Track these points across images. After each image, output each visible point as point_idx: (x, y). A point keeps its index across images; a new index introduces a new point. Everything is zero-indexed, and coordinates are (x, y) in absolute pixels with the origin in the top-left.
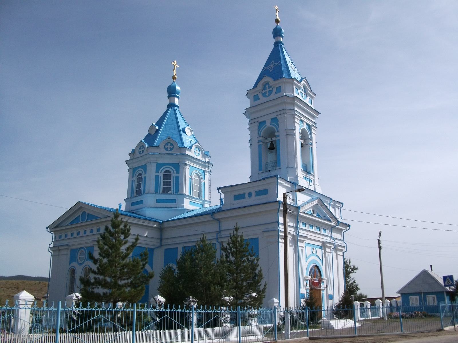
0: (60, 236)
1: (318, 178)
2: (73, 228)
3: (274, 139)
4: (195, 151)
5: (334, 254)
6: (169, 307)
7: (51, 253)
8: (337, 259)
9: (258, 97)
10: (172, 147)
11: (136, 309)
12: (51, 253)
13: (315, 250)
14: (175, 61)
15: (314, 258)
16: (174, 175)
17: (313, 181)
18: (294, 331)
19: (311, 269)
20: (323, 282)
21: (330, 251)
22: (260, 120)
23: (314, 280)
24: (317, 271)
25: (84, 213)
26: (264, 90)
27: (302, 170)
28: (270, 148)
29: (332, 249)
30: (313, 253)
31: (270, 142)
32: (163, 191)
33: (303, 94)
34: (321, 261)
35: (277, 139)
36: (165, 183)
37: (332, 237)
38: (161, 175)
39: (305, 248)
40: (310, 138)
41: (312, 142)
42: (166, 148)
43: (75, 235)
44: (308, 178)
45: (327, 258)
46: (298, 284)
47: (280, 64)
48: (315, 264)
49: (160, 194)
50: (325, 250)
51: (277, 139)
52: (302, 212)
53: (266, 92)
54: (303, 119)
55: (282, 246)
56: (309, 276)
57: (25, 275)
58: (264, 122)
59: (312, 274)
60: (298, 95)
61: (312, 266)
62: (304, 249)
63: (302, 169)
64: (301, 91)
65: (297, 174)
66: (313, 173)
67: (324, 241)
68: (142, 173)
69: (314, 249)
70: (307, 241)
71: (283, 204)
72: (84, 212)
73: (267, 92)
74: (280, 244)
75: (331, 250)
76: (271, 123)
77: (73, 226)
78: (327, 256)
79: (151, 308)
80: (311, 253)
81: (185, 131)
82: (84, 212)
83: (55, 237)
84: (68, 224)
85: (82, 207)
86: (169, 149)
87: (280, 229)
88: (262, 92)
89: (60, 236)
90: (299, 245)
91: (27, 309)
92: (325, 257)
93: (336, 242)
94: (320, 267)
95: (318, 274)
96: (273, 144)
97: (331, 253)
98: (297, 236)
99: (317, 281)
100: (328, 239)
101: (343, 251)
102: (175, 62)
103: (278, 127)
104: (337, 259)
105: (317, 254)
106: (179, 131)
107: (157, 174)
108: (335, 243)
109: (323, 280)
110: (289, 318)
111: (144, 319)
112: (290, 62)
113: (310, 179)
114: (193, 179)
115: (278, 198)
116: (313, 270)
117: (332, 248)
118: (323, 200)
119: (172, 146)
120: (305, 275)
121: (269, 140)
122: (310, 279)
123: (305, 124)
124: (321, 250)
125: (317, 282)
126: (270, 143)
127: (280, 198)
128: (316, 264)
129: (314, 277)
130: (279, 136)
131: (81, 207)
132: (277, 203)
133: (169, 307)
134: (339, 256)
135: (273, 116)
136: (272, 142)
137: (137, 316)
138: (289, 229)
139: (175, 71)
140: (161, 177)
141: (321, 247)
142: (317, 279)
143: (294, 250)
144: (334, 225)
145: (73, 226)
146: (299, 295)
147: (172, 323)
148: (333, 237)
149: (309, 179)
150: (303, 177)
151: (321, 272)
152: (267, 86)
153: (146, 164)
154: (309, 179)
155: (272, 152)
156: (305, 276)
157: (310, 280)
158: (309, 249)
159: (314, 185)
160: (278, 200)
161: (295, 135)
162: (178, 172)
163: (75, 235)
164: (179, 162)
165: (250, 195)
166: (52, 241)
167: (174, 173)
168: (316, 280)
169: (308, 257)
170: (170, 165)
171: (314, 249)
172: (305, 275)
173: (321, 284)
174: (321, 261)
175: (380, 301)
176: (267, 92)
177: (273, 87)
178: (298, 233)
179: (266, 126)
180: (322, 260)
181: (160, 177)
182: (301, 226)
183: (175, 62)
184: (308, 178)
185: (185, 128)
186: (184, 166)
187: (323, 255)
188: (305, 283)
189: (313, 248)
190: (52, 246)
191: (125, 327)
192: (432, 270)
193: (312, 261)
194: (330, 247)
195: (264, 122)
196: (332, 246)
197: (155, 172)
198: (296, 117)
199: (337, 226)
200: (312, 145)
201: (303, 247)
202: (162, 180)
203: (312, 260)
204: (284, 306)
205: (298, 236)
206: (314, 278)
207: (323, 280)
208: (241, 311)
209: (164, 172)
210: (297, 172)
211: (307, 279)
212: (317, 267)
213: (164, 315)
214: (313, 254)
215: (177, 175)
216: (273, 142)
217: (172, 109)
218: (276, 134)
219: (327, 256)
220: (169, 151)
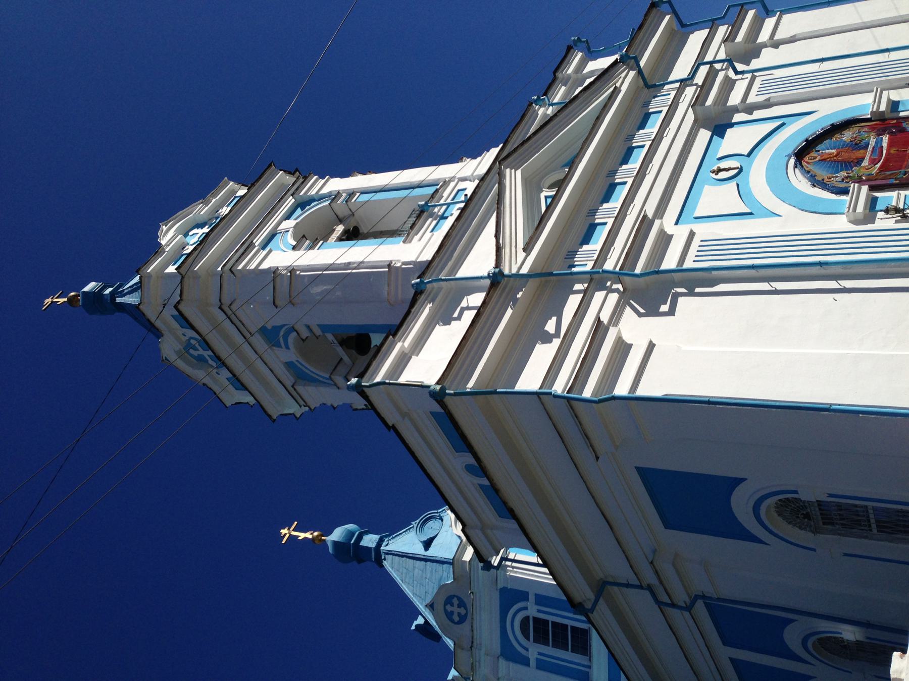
5: (768, 57)
8: (792, 40)
10: (455, 601)
13: (724, 164)
19: (816, 182)
20: (894, 105)
22: (289, 380)
23: (873, 162)
24: (827, 149)
26: (208, 361)
30: (735, 171)
34: (783, 124)
36: (560, 643)
38: (534, 651)
40: (327, 203)
41: (344, 191)
42: (462, 608)
48: (792, 161)
49: (589, 667)
52: (524, 254)
56: (845, 192)
58: (289, 365)
59: (843, 174)
61: (799, 182)
62: (704, 231)
69: (720, 170)
75: (740, 76)
78: (761, 98)
80: (732, 185)
92: (767, 105)
94: (809, 134)
95: (847, 136)
97: (756, 74)
98: (627, 279)
99: (885, 139)
104: (792, 40)
105: (746, 154)
107: (533, 663)
109: (883, 108)
113: (449, 201)
116: (822, 173)
118: (511, 148)
120: (841, 223)
122: (865, 188)
125: (890, 145)
128: (790, 157)
129: (859, 161)
135: (258, 341)
140: (540, 654)
141: (720, 130)
142: (872, 142)
143: (697, 290)
144: (632, 74)
146: (421, 613)
149: (448, 205)
151: (837, 120)
157: (872, 188)
162: (524, 596)
167: (526, 608)
168: (878, 148)
170: (505, 622)
171: (720, 170)
172: (841, 223)
173: (902, 114)
174: (783, 124)
180: (778, 123)
182: (585, 260)
184: (444, 207)
186: (506, 571)
187: (757, 114)
188: (884, 222)
194: (729, 85)
195: (289, 365)
200: (351, 194)
201: (692, 235)
205: (624, 273)
206: (866, 163)
207: (883, 108)
210: (404, 263)
212: (800, 155)
214: (741, 170)
215: (532, 598)
217: (385, 559)
219: (767, 96)
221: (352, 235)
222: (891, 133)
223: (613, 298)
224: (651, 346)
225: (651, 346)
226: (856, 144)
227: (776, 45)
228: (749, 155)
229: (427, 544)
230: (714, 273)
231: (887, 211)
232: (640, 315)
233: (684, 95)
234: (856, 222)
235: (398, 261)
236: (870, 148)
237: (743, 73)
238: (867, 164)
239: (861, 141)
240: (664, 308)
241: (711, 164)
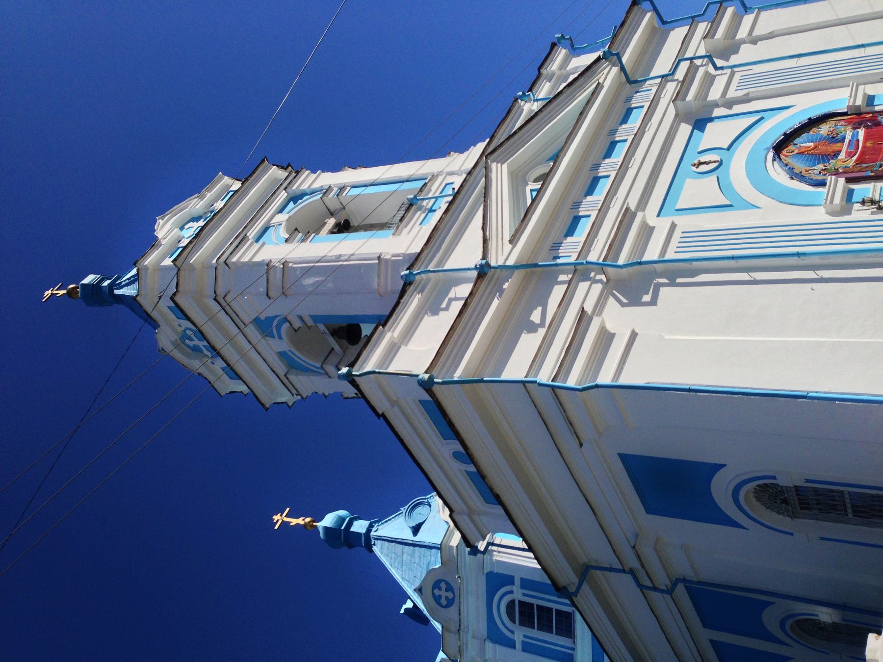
1: (296, 229)
5: (746, 53)
13: (704, 158)
16: (518, 594)
21: (725, 78)
22: (281, 369)
23: (850, 155)
24: (804, 142)
27: (393, 234)
29: (716, 68)
30: (717, 164)
34: (762, 118)
37: (665, 78)
38: (519, 634)
41: (336, 185)
44: (433, 201)
45: (753, 91)
48: (771, 154)
50: (716, 105)
56: (822, 184)
59: (821, 167)
61: (777, 174)
62: (685, 222)
65: (398, 255)
66: (427, 179)
69: (700, 163)
74: (492, 549)
75: (719, 72)
78: (741, 93)
80: (713, 178)
90: (655, 257)
92: (746, 99)
95: (824, 129)
97: (735, 69)
99: (861, 133)
106: (414, 545)
107: (519, 645)
113: (437, 194)
116: (800, 166)
117: (711, 69)
122: (842, 181)
124: (709, 126)
129: (836, 154)
134: (434, 206)
135: (252, 332)
141: (700, 124)
142: (849, 136)
154: (437, 198)
156: (822, 210)
161: (286, 261)
162: (510, 580)
167: (512, 592)
171: (700, 163)
172: (819, 214)
174: (762, 118)
177: (183, 329)
179: (290, 351)
181: (526, 640)
182: (570, 251)
184: (433, 201)
186: (492, 556)
187: (737, 109)
188: (860, 213)
189: (694, 168)
195: (282, 355)
196: (701, 72)
198: (234, 260)
199: (624, 60)
201: (673, 226)
203: (749, 174)
206: (842, 156)
207: (859, 102)
209: (513, 621)
210: (393, 256)
211: (837, 200)
212: (779, 148)
214: (721, 163)
215: (517, 581)
217: (374, 544)
220: (454, 596)
221: (343, 227)
222: (867, 127)
223: (597, 288)
224: (634, 336)
225: (634, 336)
226: (833, 137)
227: (754, 42)
228: (729, 149)
229: (416, 530)
230: (695, 263)
231: (863, 203)
232: (623, 305)
233: (665, 91)
234: (832, 213)
235: (388, 253)
236: (847, 141)
237: (722, 68)
238: (844, 157)
239: (838, 134)
240: (647, 298)
241: (692, 157)
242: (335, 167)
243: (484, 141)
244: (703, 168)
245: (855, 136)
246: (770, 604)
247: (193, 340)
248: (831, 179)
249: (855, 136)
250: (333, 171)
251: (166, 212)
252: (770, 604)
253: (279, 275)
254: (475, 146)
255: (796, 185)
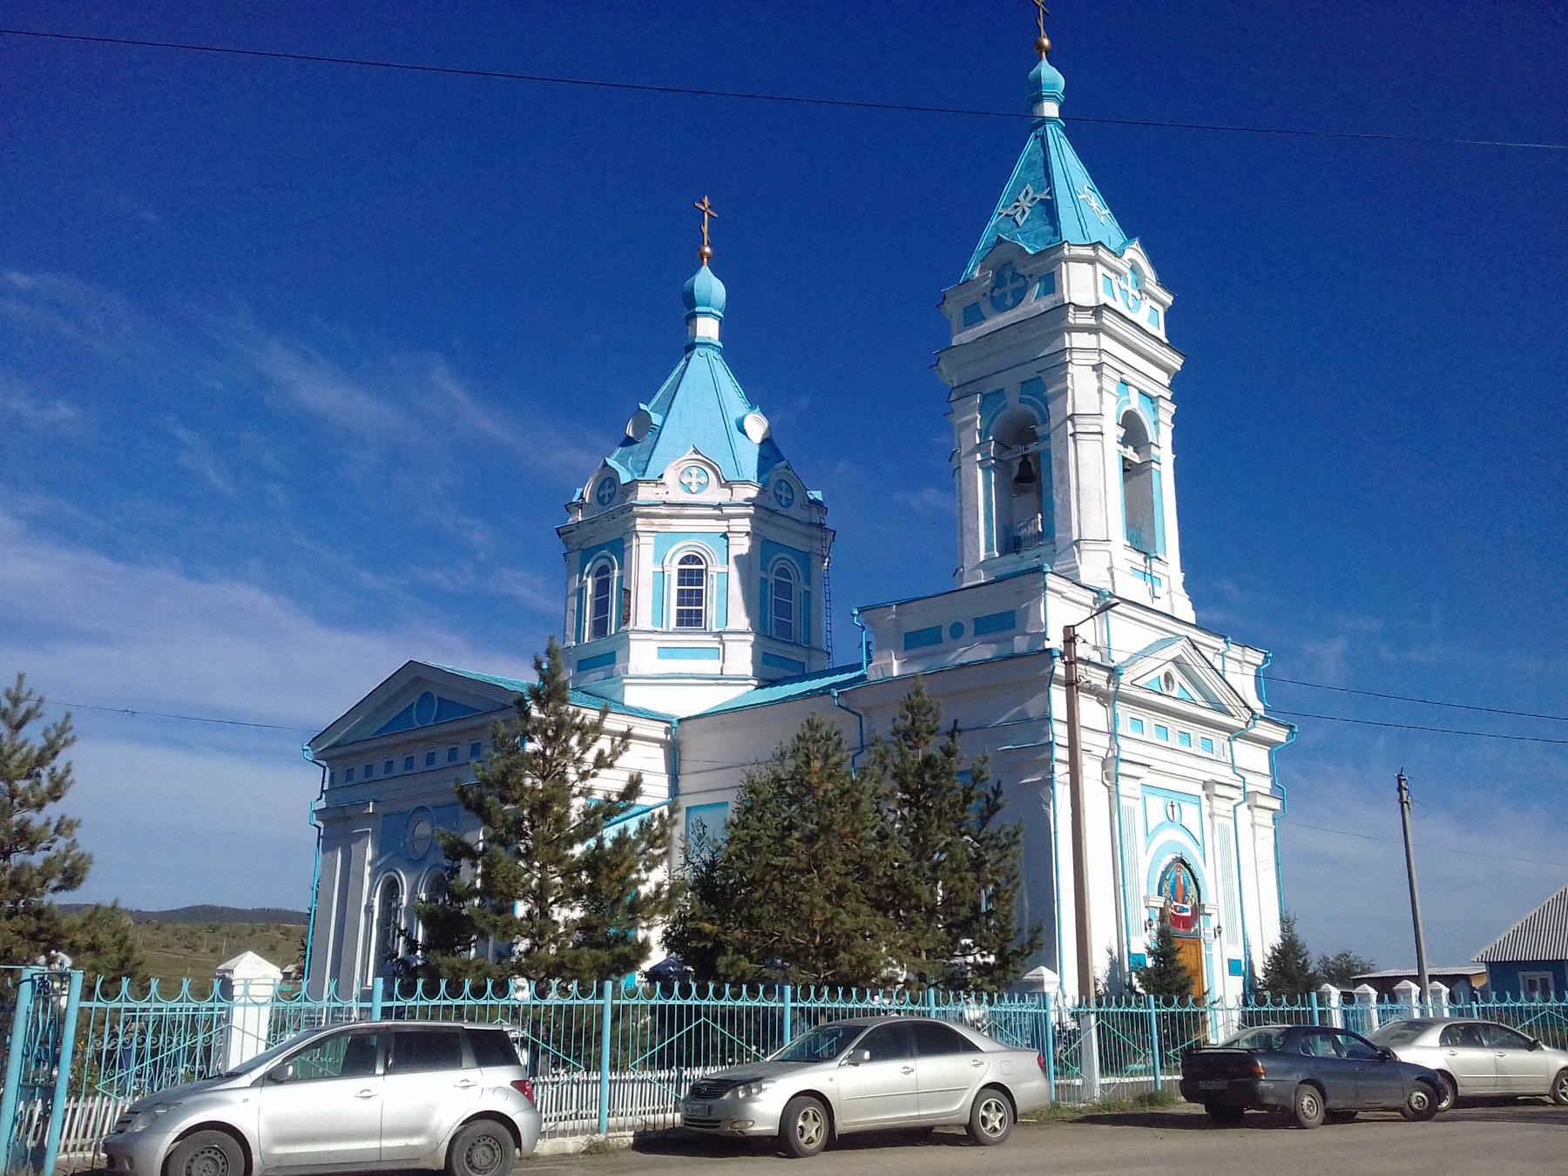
0: (349, 774)
2: (412, 741)
3: (1033, 447)
4: (779, 493)
6: (711, 991)
7: (319, 828)
9: (979, 308)
11: (612, 999)
12: (319, 828)
14: (706, 197)
15: (1173, 834)
17: (1165, 580)
18: (1112, 1079)
25: (427, 696)
26: (1000, 288)
28: (1019, 479)
31: (1018, 458)
32: (679, 623)
33: (1130, 296)
35: (1041, 447)
39: (1140, 802)
43: (399, 768)
46: (1118, 906)
47: (1049, 197)
51: (1041, 447)
53: (1006, 293)
54: (1130, 376)
55: (1062, 793)
57: (215, 904)
60: (1113, 300)
62: (1138, 806)
63: (1128, 544)
64: (1123, 286)
67: (1207, 777)
68: (610, 567)
69: (1172, 806)
70: (1151, 779)
71: (1065, 663)
72: (428, 692)
73: (1009, 296)
76: (1023, 396)
77: (392, 741)
79: (657, 995)
80: (1164, 818)
81: (743, 426)
82: (426, 694)
83: (332, 776)
84: (376, 733)
85: (420, 679)
86: (694, 488)
87: (1056, 738)
88: (991, 296)
89: (349, 774)
91: (249, 1005)
93: (1247, 781)
96: (1030, 463)
100: (1225, 774)
101: (1235, 802)
102: (706, 200)
103: (1045, 409)
108: (1244, 787)
110: (1094, 1032)
111: (653, 1021)
112: (1086, 189)
113: (1154, 574)
114: (773, 583)
115: (1048, 640)
116: (1171, 876)
119: (703, 477)
121: (1019, 450)
123: (1134, 393)
126: (1021, 460)
127: (1055, 641)
130: (1047, 437)
131: (417, 680)
132: (1047, 656)
133: (711, 991)
136: (1025, 457)
137: (568, 1043)
138: (1085, 738)
139: (705, 229)
145: (392, 741)
147: (723, 1041)
148: (1237, 764)
150: (1129, 570)
152: (1008, 273)
153: (621, 538)
154: (1151, 575)
155: (1026, 491)
157: (1161, 909)
158: (1157, 805)
159: (1168, 596)
160: (1048, 645)
163: (399, 768)
164: (727, 529)
165: (957, 630)
166: (322, 791)
169: (1152, 832)
171: (1172, 806)
175: (1413, 986)
176: (1009, 296)
178: (1118, 753)
179: (1005, 406)
183: (706, 200)
185: (743, 418)
189: (1170, 804)
190: (322, 804)
191: (578, 1058)
192: (1232, 799)
193: (1169, 844)
197: (652, 560)
202: (675, 587)
204: (1076, 993)
205: (1118, 759)
208: (937, 1004)
209: (682, 562)
213: (698, 1017)
216: (1030, 459)
218: (1039, 430)
242: (1176, 447)
243: (1167, 337)
244: (1170, 809)
245: (1187, 910)
246: (1056, 973)
247: (1022, 218)
248: (1163, 899)
249: (1187, 910)
250: (1184, 583)
251: (1442, 983)
252: (1056, 973)
253: (1059, 361)
254: (1189, 600)
255: (1159, 875)
